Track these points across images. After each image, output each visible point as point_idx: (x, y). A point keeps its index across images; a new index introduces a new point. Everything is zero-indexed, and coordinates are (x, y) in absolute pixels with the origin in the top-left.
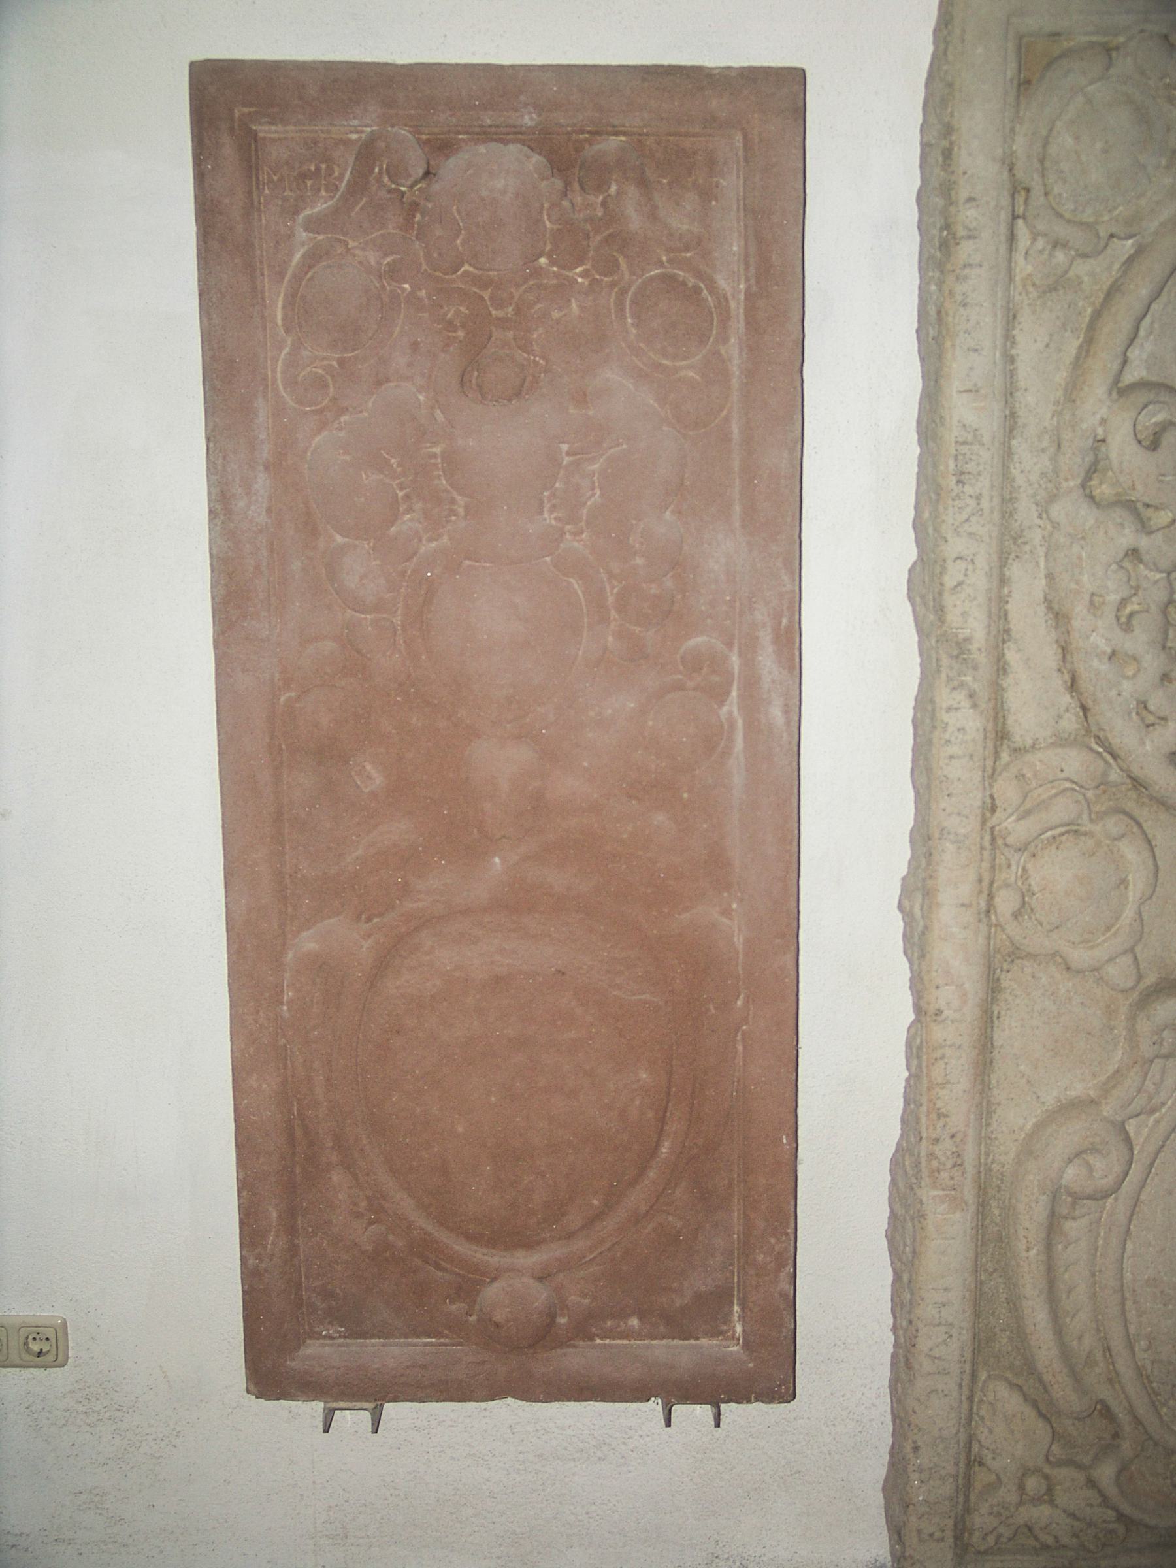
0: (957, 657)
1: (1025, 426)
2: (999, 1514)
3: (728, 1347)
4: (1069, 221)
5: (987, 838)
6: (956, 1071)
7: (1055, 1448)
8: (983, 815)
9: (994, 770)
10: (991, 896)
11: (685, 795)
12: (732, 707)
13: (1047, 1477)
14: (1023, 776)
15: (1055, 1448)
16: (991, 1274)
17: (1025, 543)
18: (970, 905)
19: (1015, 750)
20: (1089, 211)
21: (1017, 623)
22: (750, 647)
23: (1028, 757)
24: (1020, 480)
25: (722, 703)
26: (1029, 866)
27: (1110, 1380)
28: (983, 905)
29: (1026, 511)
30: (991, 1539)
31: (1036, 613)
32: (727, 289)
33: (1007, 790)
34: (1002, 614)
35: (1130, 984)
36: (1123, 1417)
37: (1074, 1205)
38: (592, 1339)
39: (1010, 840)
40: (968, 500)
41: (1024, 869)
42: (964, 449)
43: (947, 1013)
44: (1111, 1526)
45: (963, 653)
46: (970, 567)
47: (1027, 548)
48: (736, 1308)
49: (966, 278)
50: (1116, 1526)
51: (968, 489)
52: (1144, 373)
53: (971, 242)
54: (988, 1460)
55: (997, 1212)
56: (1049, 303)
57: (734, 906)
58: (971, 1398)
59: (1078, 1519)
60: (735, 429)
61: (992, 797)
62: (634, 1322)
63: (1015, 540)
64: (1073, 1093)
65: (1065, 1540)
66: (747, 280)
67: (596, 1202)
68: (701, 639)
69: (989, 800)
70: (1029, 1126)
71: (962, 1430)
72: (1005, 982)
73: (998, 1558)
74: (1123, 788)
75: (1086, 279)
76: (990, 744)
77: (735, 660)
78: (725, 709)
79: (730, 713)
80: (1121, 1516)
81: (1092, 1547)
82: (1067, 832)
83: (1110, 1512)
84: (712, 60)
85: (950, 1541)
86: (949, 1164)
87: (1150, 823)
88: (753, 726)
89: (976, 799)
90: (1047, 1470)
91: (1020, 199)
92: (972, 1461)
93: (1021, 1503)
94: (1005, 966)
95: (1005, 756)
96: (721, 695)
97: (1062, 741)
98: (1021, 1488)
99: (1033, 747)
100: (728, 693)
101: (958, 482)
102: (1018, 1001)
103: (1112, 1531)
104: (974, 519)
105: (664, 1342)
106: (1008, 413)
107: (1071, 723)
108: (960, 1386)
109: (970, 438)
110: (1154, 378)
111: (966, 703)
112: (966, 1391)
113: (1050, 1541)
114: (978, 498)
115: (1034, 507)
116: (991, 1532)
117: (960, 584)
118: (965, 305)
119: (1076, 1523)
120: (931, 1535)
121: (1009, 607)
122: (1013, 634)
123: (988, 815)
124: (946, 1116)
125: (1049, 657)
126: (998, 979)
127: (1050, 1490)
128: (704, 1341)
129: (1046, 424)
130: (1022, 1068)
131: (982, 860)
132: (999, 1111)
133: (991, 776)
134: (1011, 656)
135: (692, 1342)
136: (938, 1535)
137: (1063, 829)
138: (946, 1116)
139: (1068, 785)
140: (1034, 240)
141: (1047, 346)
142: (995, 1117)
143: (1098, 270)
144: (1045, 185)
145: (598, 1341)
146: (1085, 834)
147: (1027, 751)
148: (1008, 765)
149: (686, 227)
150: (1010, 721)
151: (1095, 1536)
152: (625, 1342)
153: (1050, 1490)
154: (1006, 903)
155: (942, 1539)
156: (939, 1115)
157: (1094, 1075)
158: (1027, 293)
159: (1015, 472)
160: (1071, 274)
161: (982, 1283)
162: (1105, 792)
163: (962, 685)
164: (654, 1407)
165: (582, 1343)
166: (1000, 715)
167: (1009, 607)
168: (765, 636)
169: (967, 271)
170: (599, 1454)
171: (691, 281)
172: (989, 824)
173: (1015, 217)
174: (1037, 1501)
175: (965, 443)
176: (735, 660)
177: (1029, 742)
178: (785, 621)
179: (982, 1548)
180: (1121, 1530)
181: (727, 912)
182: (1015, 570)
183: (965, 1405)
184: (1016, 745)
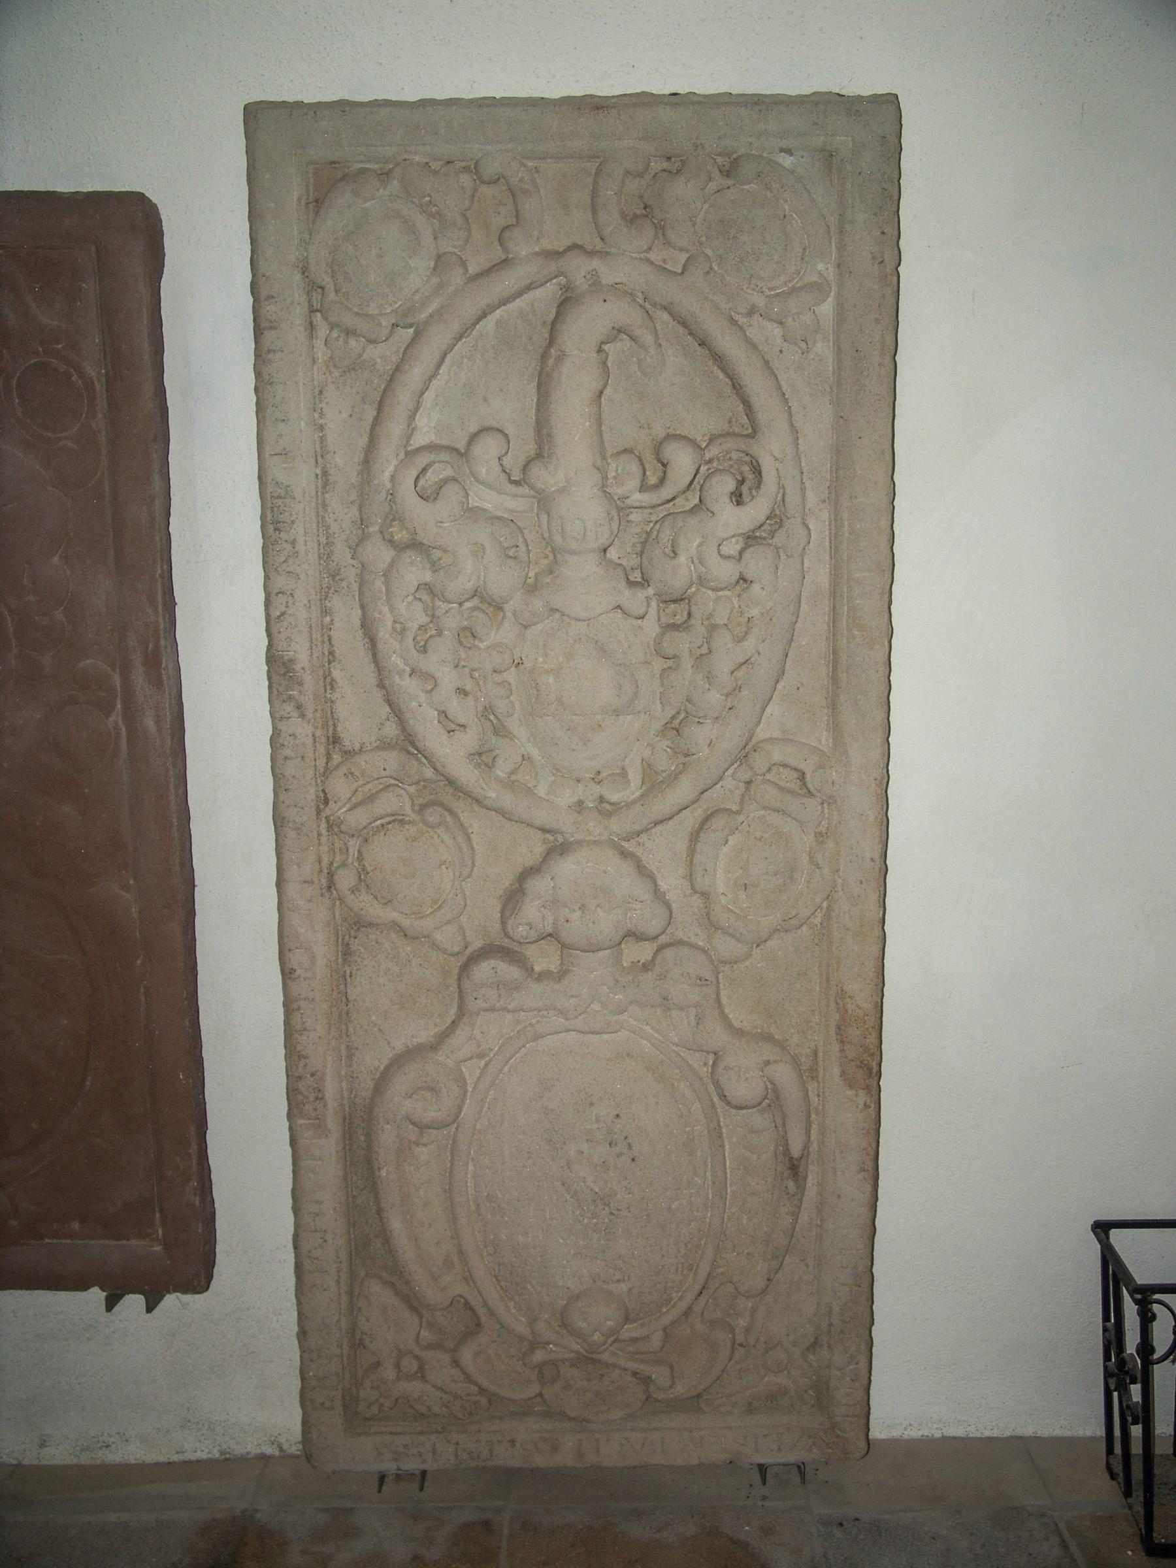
0: (284, 675)
1: (336, 482)
2: (378, 1388)
3: (148, 1248)
4: (357, 314)
5: (324, 825)
6: (315, 1021)
7: (424, 1333)
8: (318, 807)
9: (326, 768)
10: (331, 875)
11: (87, 791)
12: (116, 718)
13: (417, 1357)
14: (352, 774)
15: (424, 1333)
16: (362, 1190)
17: (342, 580)
18: (312, 882)
19: (346, 752)
20: (373, 305)
21: (340, 648)
22: (126, 669)
23: (358, 759)
24: (334, 527)
25: (108, 715)
26: (363, 850)
27: (466, 1280)
28: (324, 881)
29: (341, 554)
30: (375, 1409)
31: (355, 638)
32: (93, 374)
33: (340, 787)
34: (326, 638)
35: (456, 949)
36: (481, 1311)
37: (421, 1134)
38: (42, 1238)
39: (343, 828)
40: (285, 545)
41: (359, 852)
42: (279, 502)
43: (298, 972)
44: (474, 1398)
45: (288, 672)
46: (290, 600)
47: (344, 584)
48: (158, 1215)
49: (270, 361)
50: (478, 1398)
51: (283, 535)
52: (433, 438)
53: (273, 332)
54: (367, 1343)
55: (362, 1138)
56: (349, 381)
57: (131, 882)
58: (350, 1293)
59: (446, 1393)
60: (107, 488)
61: (323, 791)
62: (76, 1225)
63: (333, 577)
64: (419, 1040)
65: (436, 1409)
66: (106, 366)
67: (34, 1125)
68: (88, 662)
69: (322, 795)
70: (382, 1068)
71: (343, 1318)
72: (354, 948)
73: (383, 1423)
74: (442, 784)
75: (378, 360)
76: (322, 749)
77: (117, 681)
78: (111, 719)
79: (116, 722)
80: (482, 1390)
81: (460, 1416)
82: (394, 821)
83: (473, 1387)
84: (63, 187)
85: (339, 1409)
86: (312, 1099)
87: (466, 814)
88: (131, 732)
89: (311, 793)
90: (417, 1351)
91: (316, 296)
92: (357, 1343)
93: (398, 1379)
94: (353, 934)
95: (337, 758)
96: (108, 709)
97: (384, 745)
98: (398, 1366)
99: (361, 749)
100: (113, 706)
101: (275, 529)
102: (366, 962)
103: (476, 1402)
104: (291, 561)
105: (102, 1242)
106: (318, 471)
107: (391, 730)
108: (338, 1282)
109: (283, 493)
110: (444, 442)
111: (295, 714)
112: (344, 1288)
113: (424, 1410)
114: (294, 542)
115: (347, 550)
116: (374, 1403)
117: (283, 614)
118: (271, 384)
119: (445, 1396)
120: (323, 1404)
121: (332, 633)
122: (337, 655)
123: (322, 806)
124: (306, 1057)
125: (369, 675)
126: (348, 944)
127: (421, 1369)
128: (134, 1242)
129: (353, 481)
130: (374, 1018)
131: (320, 844)
132: (357, 1054)
133: (327, 772)
134: (336, 674)
135: (124, 1242)
136: (328, 1404)
137: (390, 819)
138: (306, 1057)
139: (393, 782)
140: (332, 329)
141: (351, 416)
142: (355, 1059)
143: (388, 353)
144: (335, 284)
145: (47, 1240)
146: (410, 822)
147: (356, 754)
148: (338, 766)
149: (55, 323)
150: (339, 729)
151: (462, 1406)
152: (69, 1241)
153: (421, 1369)
154: (346, 880)
155: (332, 1408)
156: (300, 1057)
157: (436, 1025)
158: (331, 373)
159: (330, 521)
160: (365, 356)
161: (354, 1197)
162: (425, 787)
163: (290, 698)
164: (97, 1295)
165: (32, 1242)
166: (331, 723)
167: (332, 633)
168: (137, 659)
169: (271, 355)
170: (88, 1335)
171: (63, 368)
172: (323, 815)
173: (312, 311)
174: (410, 1377)
175: (279, 497)
176: (117, 681)
177: (357, 746)
178: (151, 646)
179: (368, 1415)
180: (484, 1401)
181: (126, 887)
182: (336, 603)
183: (344, 1298)
184: (346, 748)
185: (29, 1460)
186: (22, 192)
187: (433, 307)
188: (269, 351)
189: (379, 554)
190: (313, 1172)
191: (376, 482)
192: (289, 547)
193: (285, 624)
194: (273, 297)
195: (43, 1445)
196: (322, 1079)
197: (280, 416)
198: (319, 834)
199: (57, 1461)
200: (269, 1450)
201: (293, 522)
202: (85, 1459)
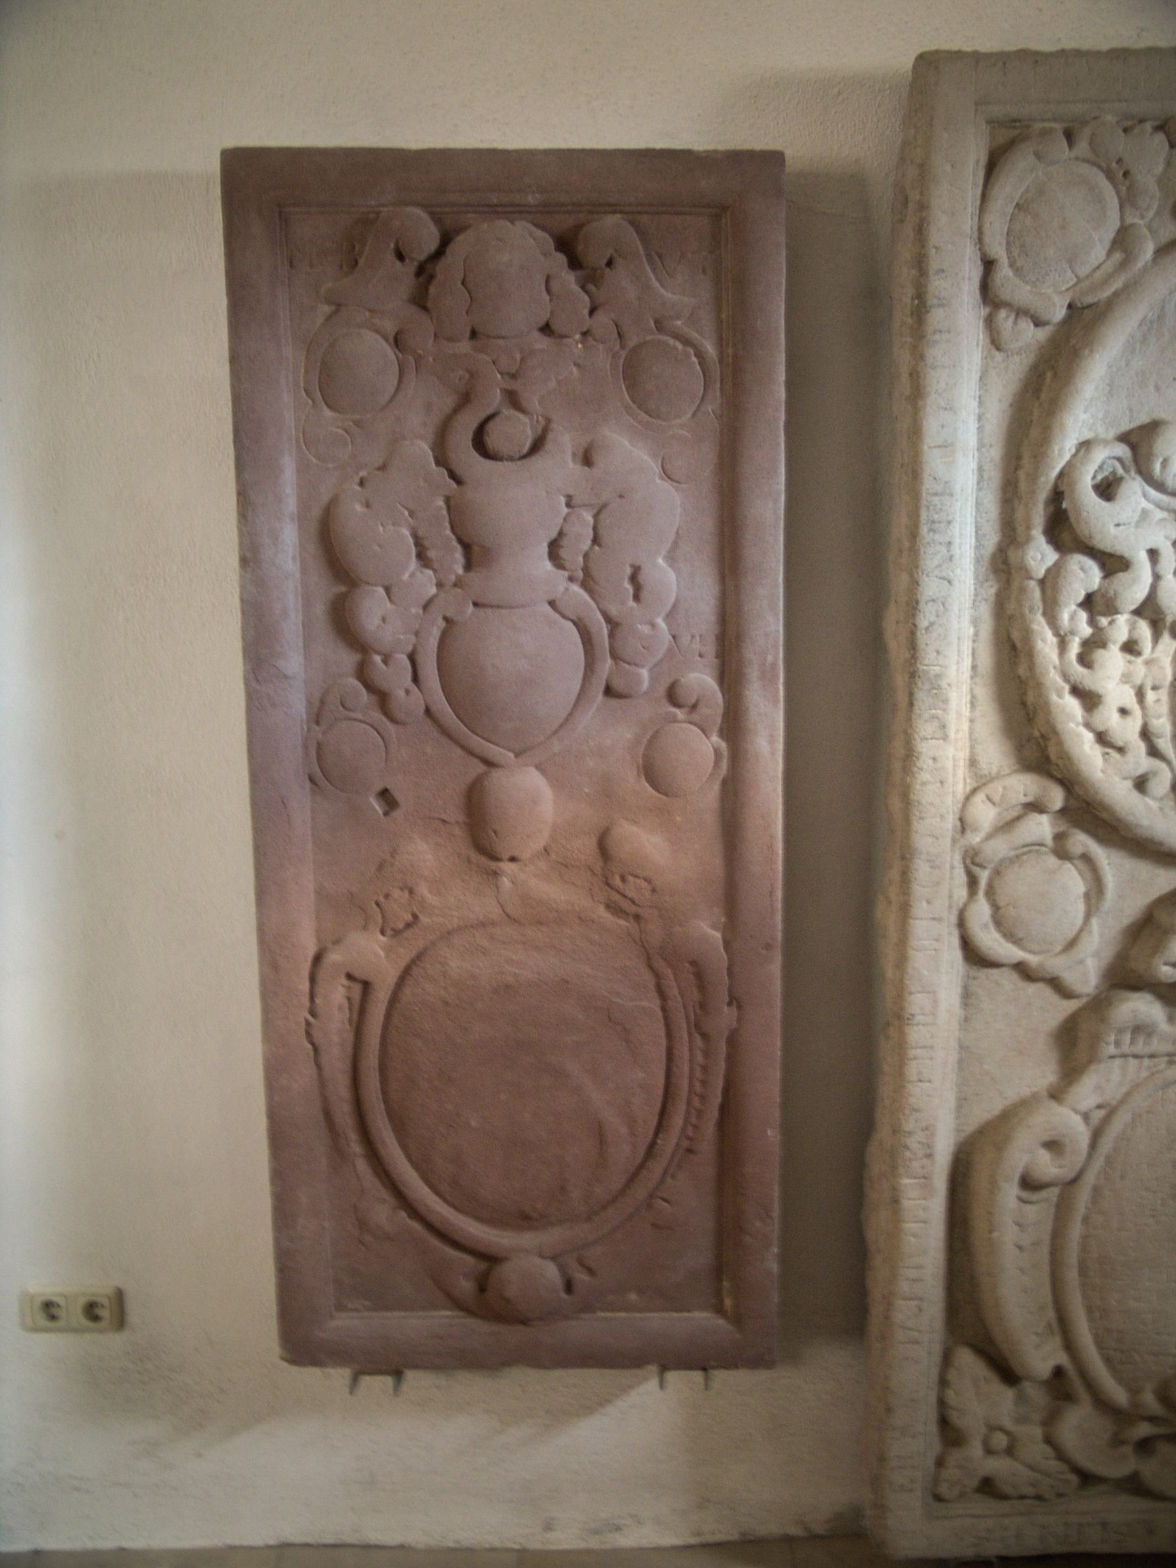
53: (941, 310)
62: (633, 1297)
82: (1030, 852)
185: (534, 1545)
186: (654, 150)
187: (1117, 284)
188: (935, 332)
189: (1040, 555)
190: (914, 1236)
191: (1042, 479)
192: (944, 549)
193: (934, 635)
194: (943, 271)
195: (548, 1527)
196: (933, 1135)
197: (943, 404)
198: (952, 867)
199: (565, 1546)
200: (793, 1530)
201: (949, 522)
202: (594, 1543)
